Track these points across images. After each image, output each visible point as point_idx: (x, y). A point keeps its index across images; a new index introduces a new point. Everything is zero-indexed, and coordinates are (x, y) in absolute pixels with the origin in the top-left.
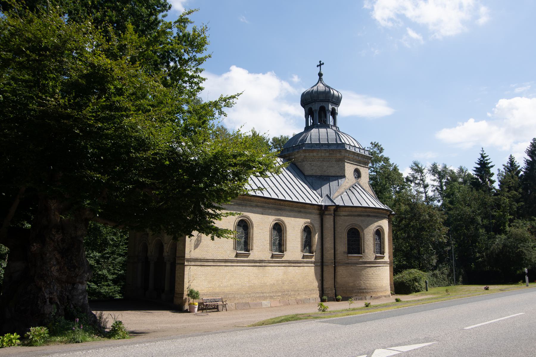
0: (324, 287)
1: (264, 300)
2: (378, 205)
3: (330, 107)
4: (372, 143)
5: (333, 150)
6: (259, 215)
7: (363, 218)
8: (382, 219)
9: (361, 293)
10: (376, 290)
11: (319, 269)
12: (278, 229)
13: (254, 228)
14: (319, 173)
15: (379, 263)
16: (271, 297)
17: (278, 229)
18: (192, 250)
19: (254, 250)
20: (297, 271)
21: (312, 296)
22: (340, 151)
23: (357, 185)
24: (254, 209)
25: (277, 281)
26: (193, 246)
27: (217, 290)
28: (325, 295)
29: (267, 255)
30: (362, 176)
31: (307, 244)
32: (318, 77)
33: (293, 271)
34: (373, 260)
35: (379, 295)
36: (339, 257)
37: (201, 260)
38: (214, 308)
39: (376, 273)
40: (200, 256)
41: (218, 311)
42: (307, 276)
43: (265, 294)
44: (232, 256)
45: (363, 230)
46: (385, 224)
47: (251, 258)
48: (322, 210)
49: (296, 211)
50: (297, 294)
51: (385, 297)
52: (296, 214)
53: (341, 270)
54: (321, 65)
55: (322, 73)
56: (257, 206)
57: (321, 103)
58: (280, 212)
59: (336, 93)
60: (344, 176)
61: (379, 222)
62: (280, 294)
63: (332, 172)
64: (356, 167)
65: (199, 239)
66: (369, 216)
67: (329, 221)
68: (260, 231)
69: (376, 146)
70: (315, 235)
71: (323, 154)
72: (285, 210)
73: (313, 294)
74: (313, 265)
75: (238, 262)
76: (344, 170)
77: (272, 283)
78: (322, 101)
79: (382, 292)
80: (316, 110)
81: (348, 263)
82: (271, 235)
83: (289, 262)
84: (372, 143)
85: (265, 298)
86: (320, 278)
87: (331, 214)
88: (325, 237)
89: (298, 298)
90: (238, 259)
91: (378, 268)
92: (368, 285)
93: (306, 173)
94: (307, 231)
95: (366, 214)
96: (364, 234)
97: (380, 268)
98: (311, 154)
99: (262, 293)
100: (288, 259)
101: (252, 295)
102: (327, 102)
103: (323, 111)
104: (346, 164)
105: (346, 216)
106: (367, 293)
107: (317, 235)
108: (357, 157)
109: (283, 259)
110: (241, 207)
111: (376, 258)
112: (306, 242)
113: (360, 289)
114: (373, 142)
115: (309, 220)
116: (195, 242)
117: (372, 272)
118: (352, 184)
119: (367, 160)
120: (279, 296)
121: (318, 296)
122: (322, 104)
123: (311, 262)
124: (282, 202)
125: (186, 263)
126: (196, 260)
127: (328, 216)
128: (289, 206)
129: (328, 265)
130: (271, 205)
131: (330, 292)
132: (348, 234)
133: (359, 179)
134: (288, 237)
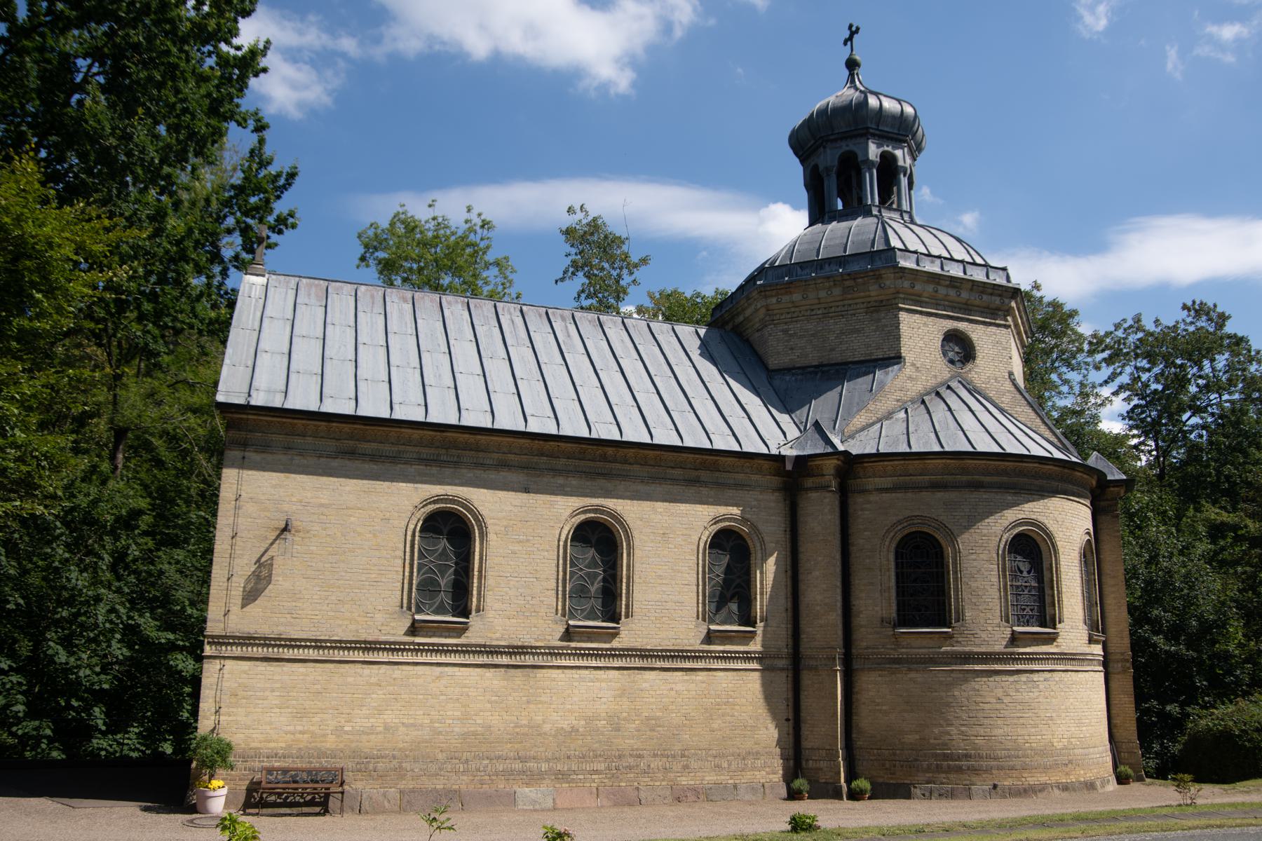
0: (806, 744)
1: (528, 785)
2: (1039, 446)
3: (874, 151)
4: (1185, 307)
5: (853, 276)
6: (511, 494)
7: (952, 495)
8: (1043, 497)
9: (950, 770)
10: (1017, 763)
11: (782, 682)
12: (599, 542)
13: (491, 537)
14: (813, 358)
15: (1032, 658)
16: (561, 776)
17: (599, 542)
18: (235, 609)
19: (490, 614)
20: (679, 687)
21: (748, 776)
22: (877, 276)
23: (954, 384)
24: (492, 475)
25: (589, 720)
26: (237, 594)
27: (330, 743)
28: (802, 773)
29: (545, 627)
30: (980, 355)
31: (729, 589)
32: (847, 73)
33: (656, 686)
34: (999, 647)
35: (1032, 781)
36: (867, 637)
37: (266, 642)
38: (311, 803)
39: (1019, 697)
40: (265, 630)
41: (326, 811)
42: (737, 700)
43: (531, 765)
44: (397, 630)
45: (953, 538)
46: (1068, 522)
47: (471, 638)
48: (790, 477)
49: (674, 481)
50: (677, 766)
51: (1065, 788)
52: (641, 487)
53: (872, 685)
54: (853, 32)
55: (858, 58)
56: (503, 465)
57: (843, 144)
58: (602, 482)
59: (888, 104)
60: (897, 359)
61: (1027, 506)
62: (602, 766)
63: (856, 348)
64: (950, 325)
65: (264, 573)
66: (977, 486)
67: (820, 512)
68: (517, 548)
69: (1198, 313)
70: (764, 559)
71: (822, 294)
72: (624, 477)
73: (754, 768)
74: (755, 665)
75: (419, 649)
76: (898, 338)
77: (565, 725)
78: (846, 136)
79: (1046, 769)
80: (828, 169)
81: (897, 661)
82: (708, 570)
83: (644, 654)
84: (1185, 307)
85: (533, 778)
86: (785, 710)
87: (825, 488)
88: (804, 565)
89: (684, 781)
90: (418, 640)
91: (1024, 677)
92: (979, 741)
93: (771, 367)
94: (730, 547)
95: (965, 478)
96: (956, 552)
97: (1035, 677)
98: (786, 298)
99: (523, 760)
100: (638, 645)
101: (472, 765)
102: (862, 135)
103: (851, 168)
104: (903, 316)
105: (886, 490)
106: (976, 771)
107: (771, 561)
108: (952, 293)
109: (615, 644)
110: (434, 470)
111: (1014, 639)
112: (727, 583)
113: (946, 757)
114: (1189, 304)
115: (735, 511)
116: (248, 581)
117: (999, 692)
118: (932, 383)
119: (997, 301)
120: (596, 772)
121: (777, 776)
122: (845, 147)
123: (747, 657)
124: (610, 451)
125: (208, 650)
126: (247, 640)
127: (814, 495)
128: (644, 463)
129: (816, 669)
130: (563, 461)
131: (823, 764)
132: (898, 555)
133: (969, 366)
134: (638, 567)
